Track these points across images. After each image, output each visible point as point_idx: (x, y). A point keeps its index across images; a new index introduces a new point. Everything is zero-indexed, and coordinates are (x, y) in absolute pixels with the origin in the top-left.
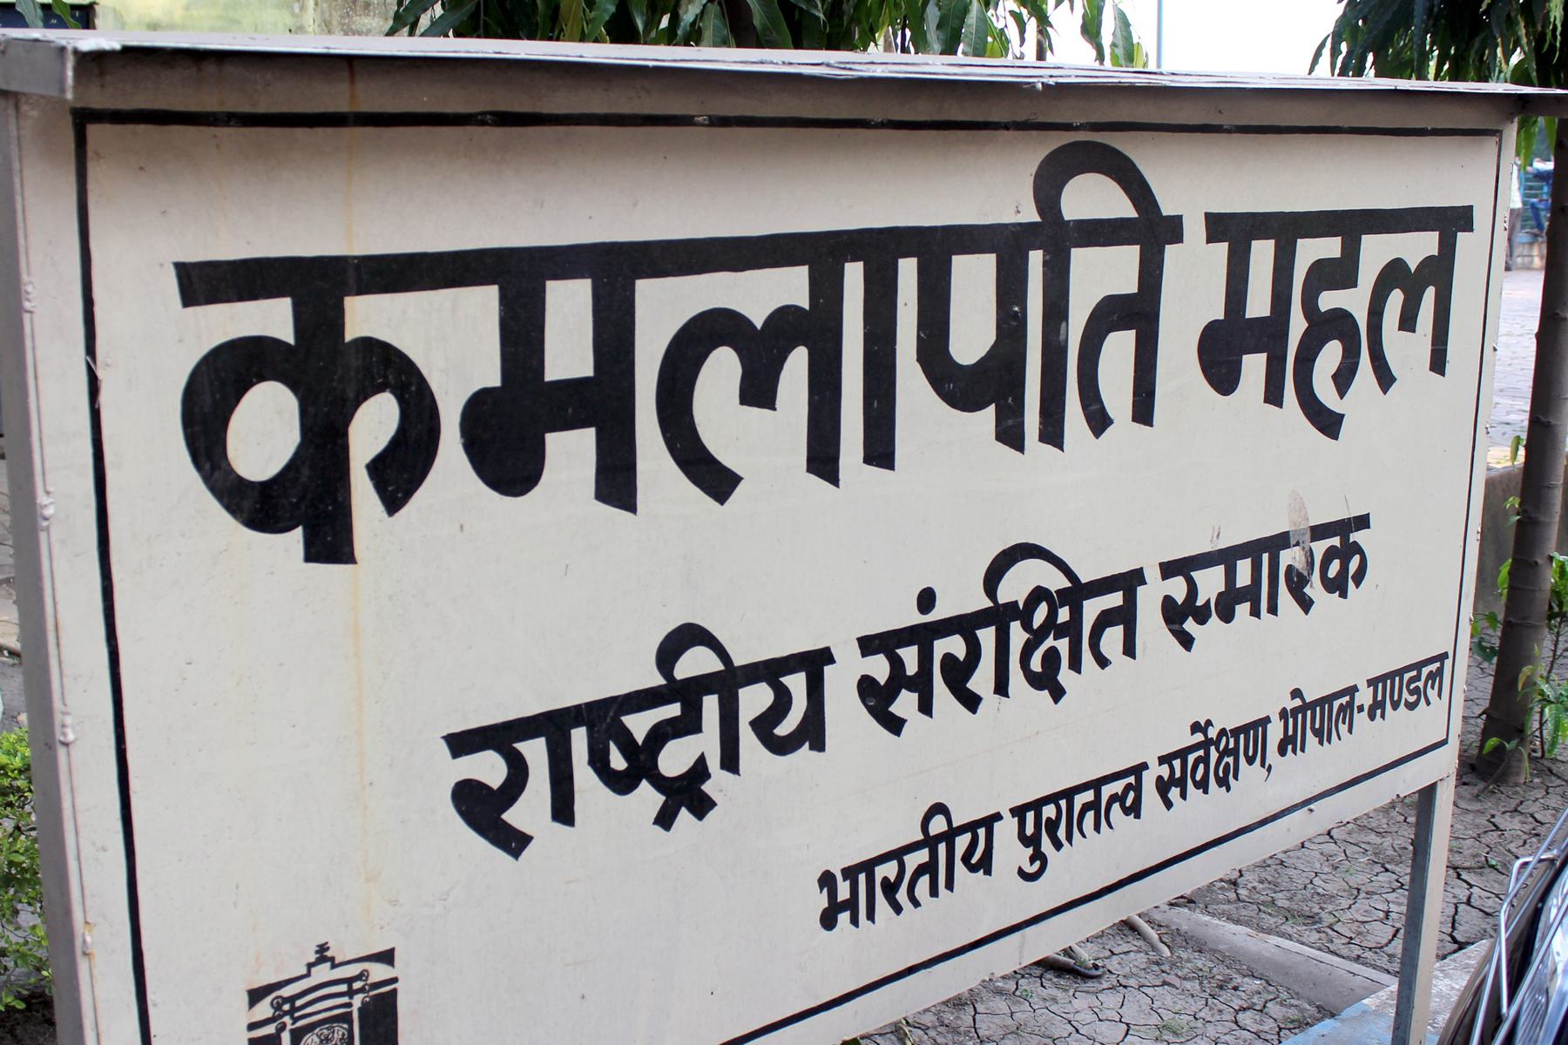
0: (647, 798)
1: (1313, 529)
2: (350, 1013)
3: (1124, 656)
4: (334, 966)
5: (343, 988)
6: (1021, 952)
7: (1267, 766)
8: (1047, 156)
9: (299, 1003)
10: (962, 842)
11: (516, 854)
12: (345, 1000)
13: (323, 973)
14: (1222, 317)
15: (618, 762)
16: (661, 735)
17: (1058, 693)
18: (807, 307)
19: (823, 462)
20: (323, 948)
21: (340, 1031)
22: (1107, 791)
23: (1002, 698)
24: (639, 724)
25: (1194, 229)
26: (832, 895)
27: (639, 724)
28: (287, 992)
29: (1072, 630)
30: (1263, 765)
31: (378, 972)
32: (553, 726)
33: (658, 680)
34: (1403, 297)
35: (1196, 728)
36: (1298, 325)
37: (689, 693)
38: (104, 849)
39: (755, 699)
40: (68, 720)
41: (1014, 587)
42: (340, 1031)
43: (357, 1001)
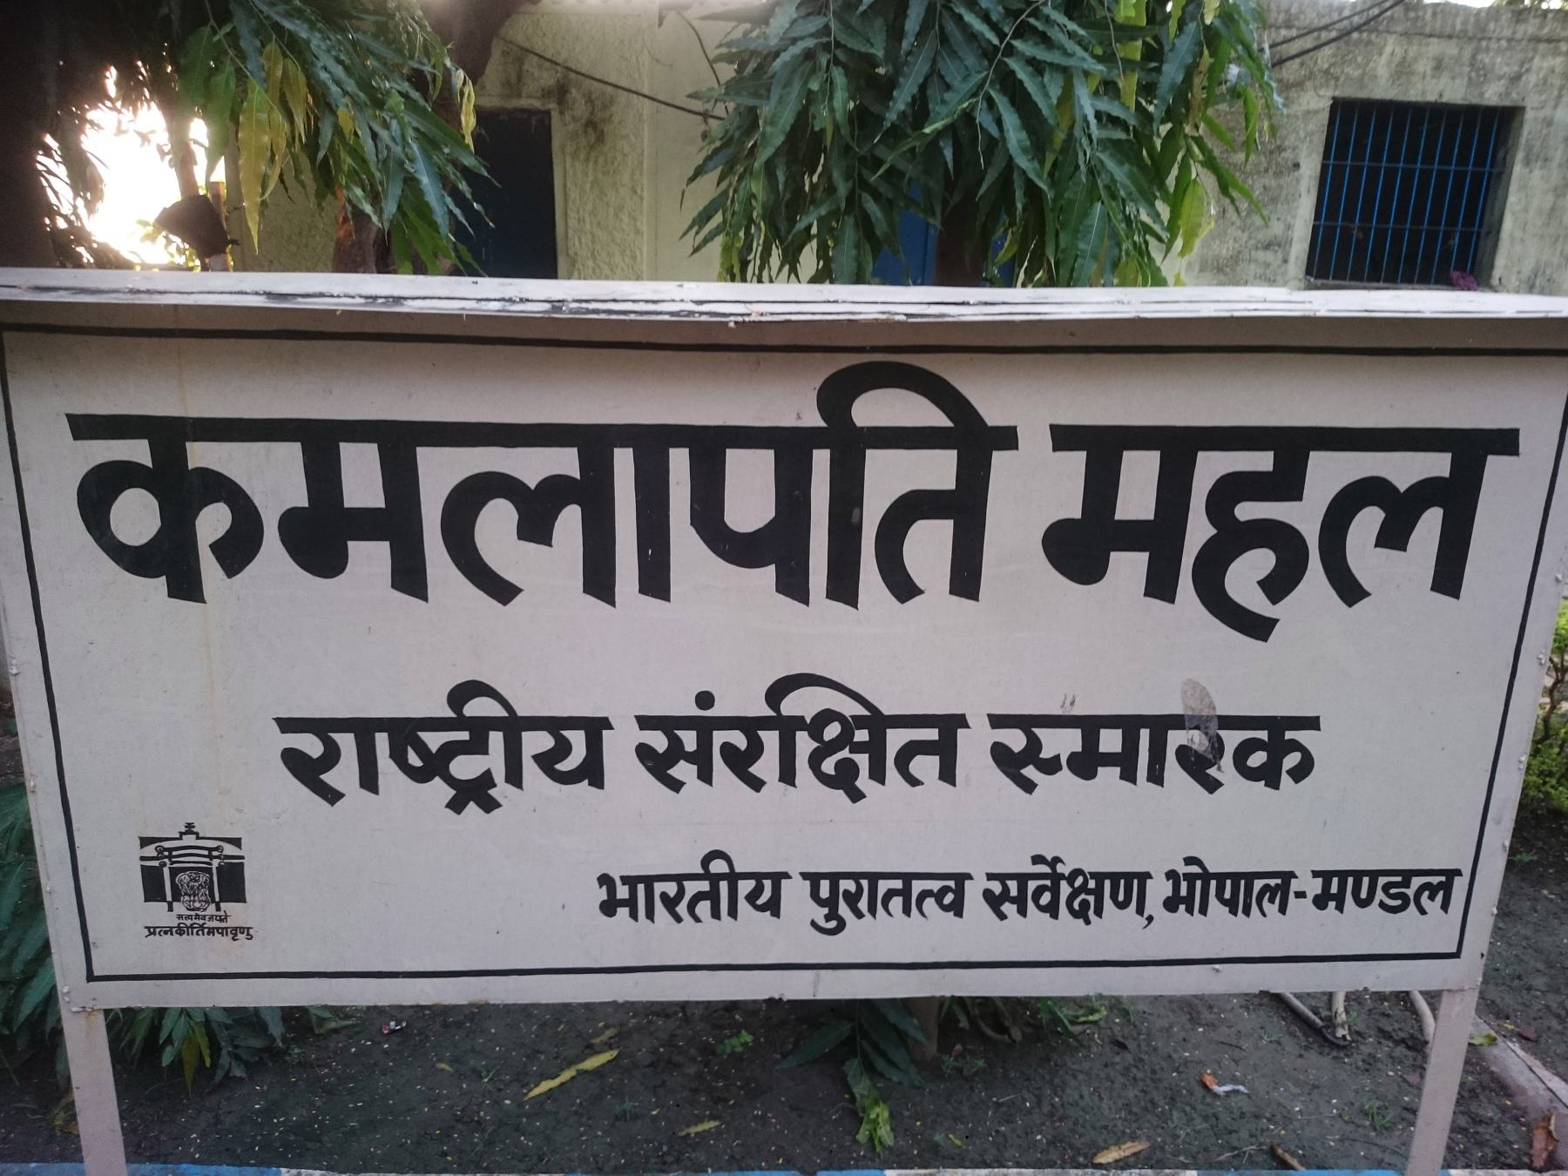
0: (439, 790)
1: (1220, 718)
2: (211, 869)
3: (941, 783)
4: (198, 838)
5: (206, 853)
6: (815, 987)
7: (1146, 915)
8: (834, 374)
9: (174, 853)
10: (745, 887)
11: (1211, 791)
12: (207, 860)
13: (189, 840)
14: (1077, 514)
15: (414, 760)
16: (451, 750)
17: (856, 795)
18: (578, 476)
19: (599, 581)
20: (190, 826)
21: (203, 878)
22: (918, 886)
23: (789, 787)
24: (434, 740)
25: (1034, 439)
26: (1176, 888)
27: (434, 740)
28: (167, 844)
29: (876, 749)
30: (1140, 911)
31: (229, 850)
32: (364, 729)
33: (449, 713)
34: (516, 516)
35: (1038, 859)
36: (1199, 531)
37: (481, 727)
38: (40, 736)
39: (536, 742)
40: (14, 662)
41: (802, 704)
42: (203, 878)
43: (216, 863)
